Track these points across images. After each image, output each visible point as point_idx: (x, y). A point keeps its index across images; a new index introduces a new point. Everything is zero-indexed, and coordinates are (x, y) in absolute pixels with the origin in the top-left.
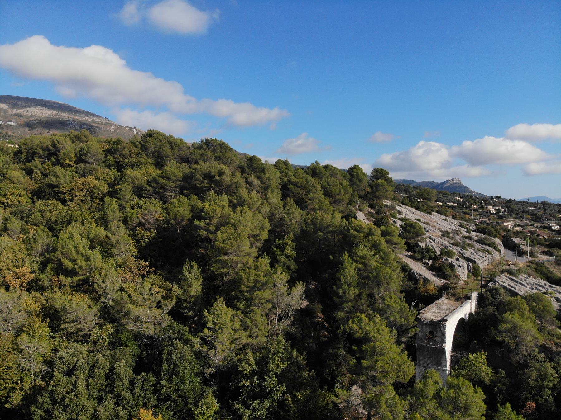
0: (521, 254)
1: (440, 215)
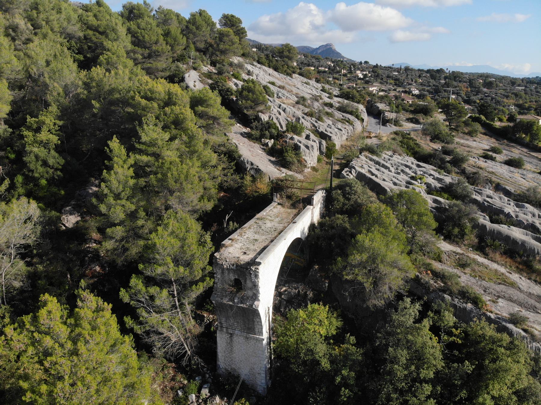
0: (385, 122)
1: (302, 78)
